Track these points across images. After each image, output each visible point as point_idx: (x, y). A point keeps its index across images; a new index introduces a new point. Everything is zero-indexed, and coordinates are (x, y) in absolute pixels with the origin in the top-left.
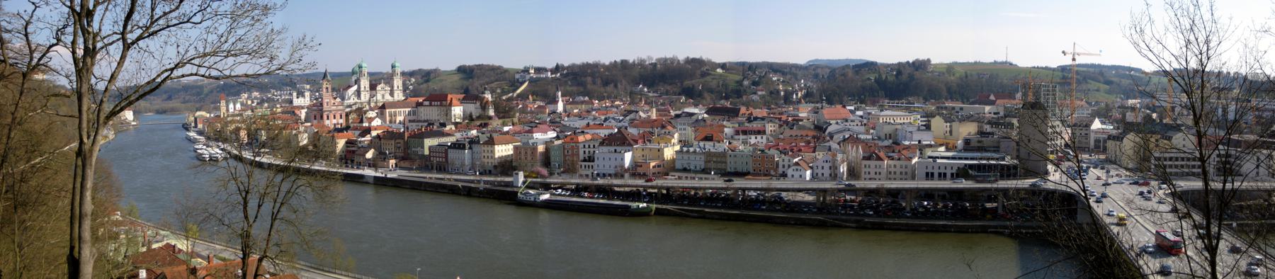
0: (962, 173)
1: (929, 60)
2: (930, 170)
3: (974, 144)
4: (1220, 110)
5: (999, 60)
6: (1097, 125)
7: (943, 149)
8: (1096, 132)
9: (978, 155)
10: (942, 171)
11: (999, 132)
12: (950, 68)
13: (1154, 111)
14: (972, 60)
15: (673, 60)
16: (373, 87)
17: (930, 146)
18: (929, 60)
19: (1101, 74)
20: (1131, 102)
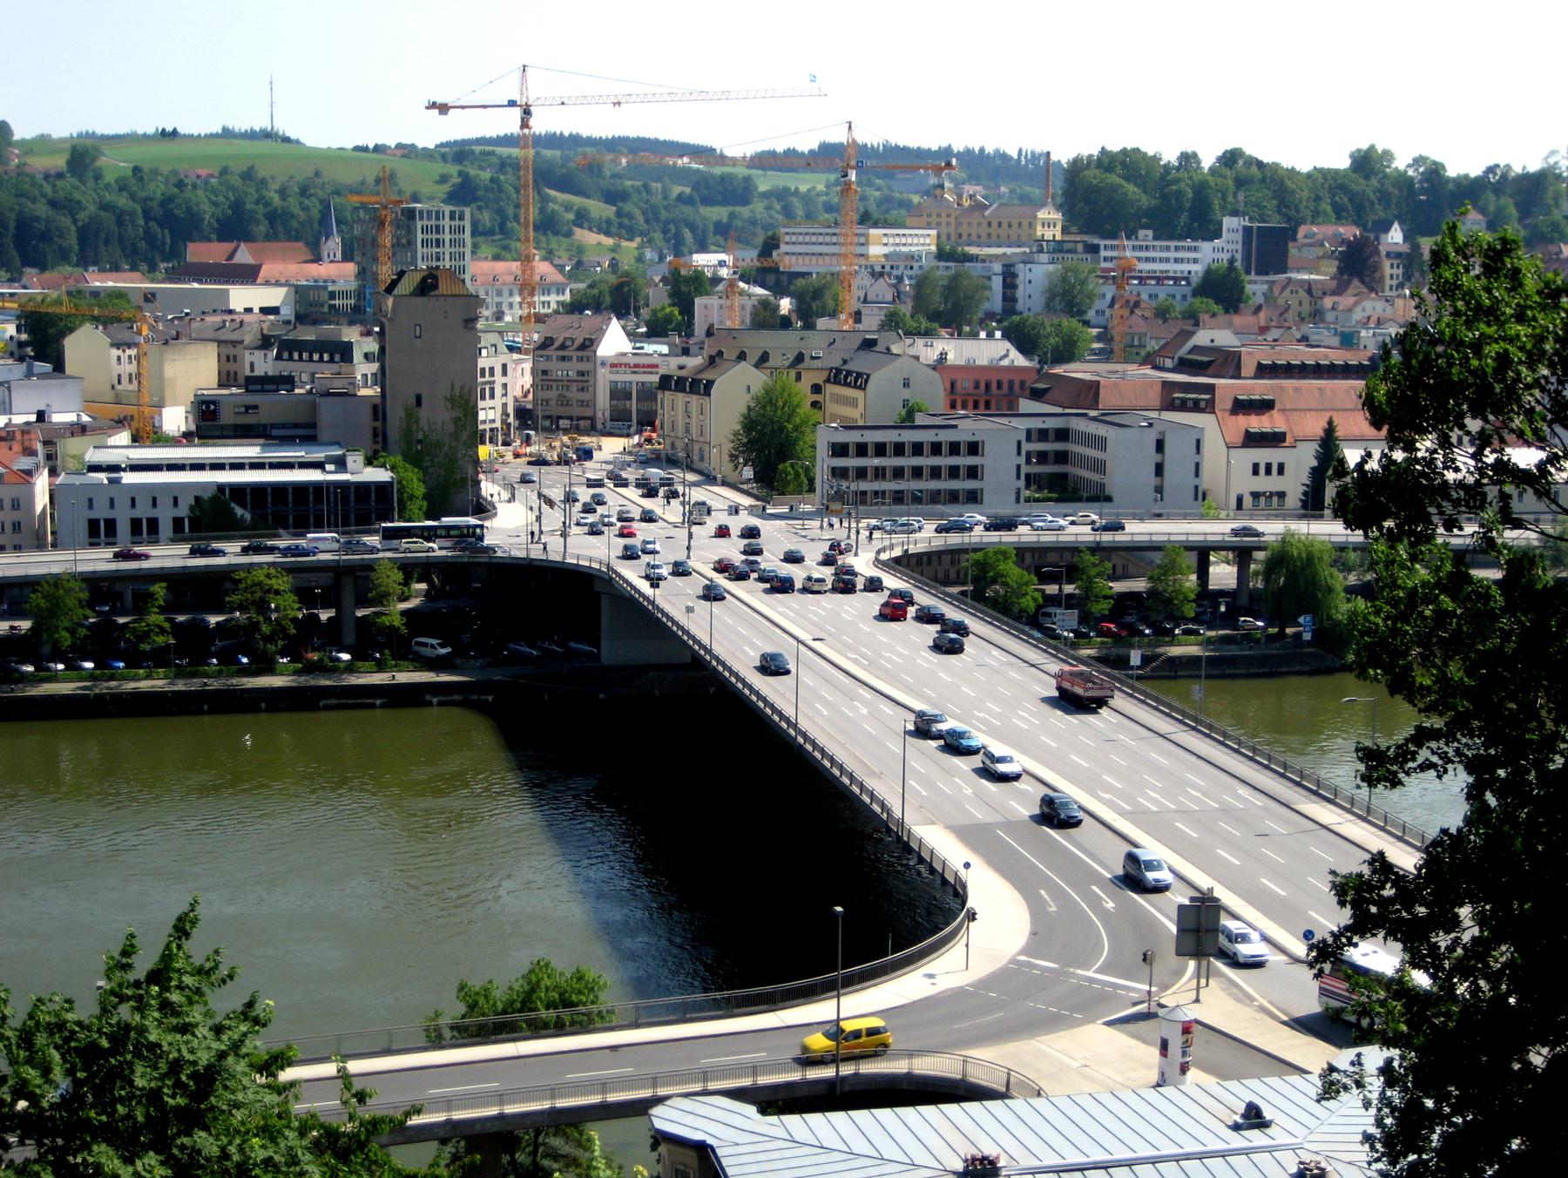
0: (211, 515)
1: (1372, 148)
2: (101, 512)
3: (227, 417)
4: (997, 282)
5: (241, 124)
6: (614, 341)
7: (123, 437)
8: (615, 365)
9: (251, 451)
10: (143, 511)
11: (309, 376)
12: (82, 155)
13: (779, 290)
14: (652, 136)
15: (1466, 176)
16: (1069, 602)
17: (80, 429)
18: (1372, 148)
19: (594, 168)
20: (704, 260)
